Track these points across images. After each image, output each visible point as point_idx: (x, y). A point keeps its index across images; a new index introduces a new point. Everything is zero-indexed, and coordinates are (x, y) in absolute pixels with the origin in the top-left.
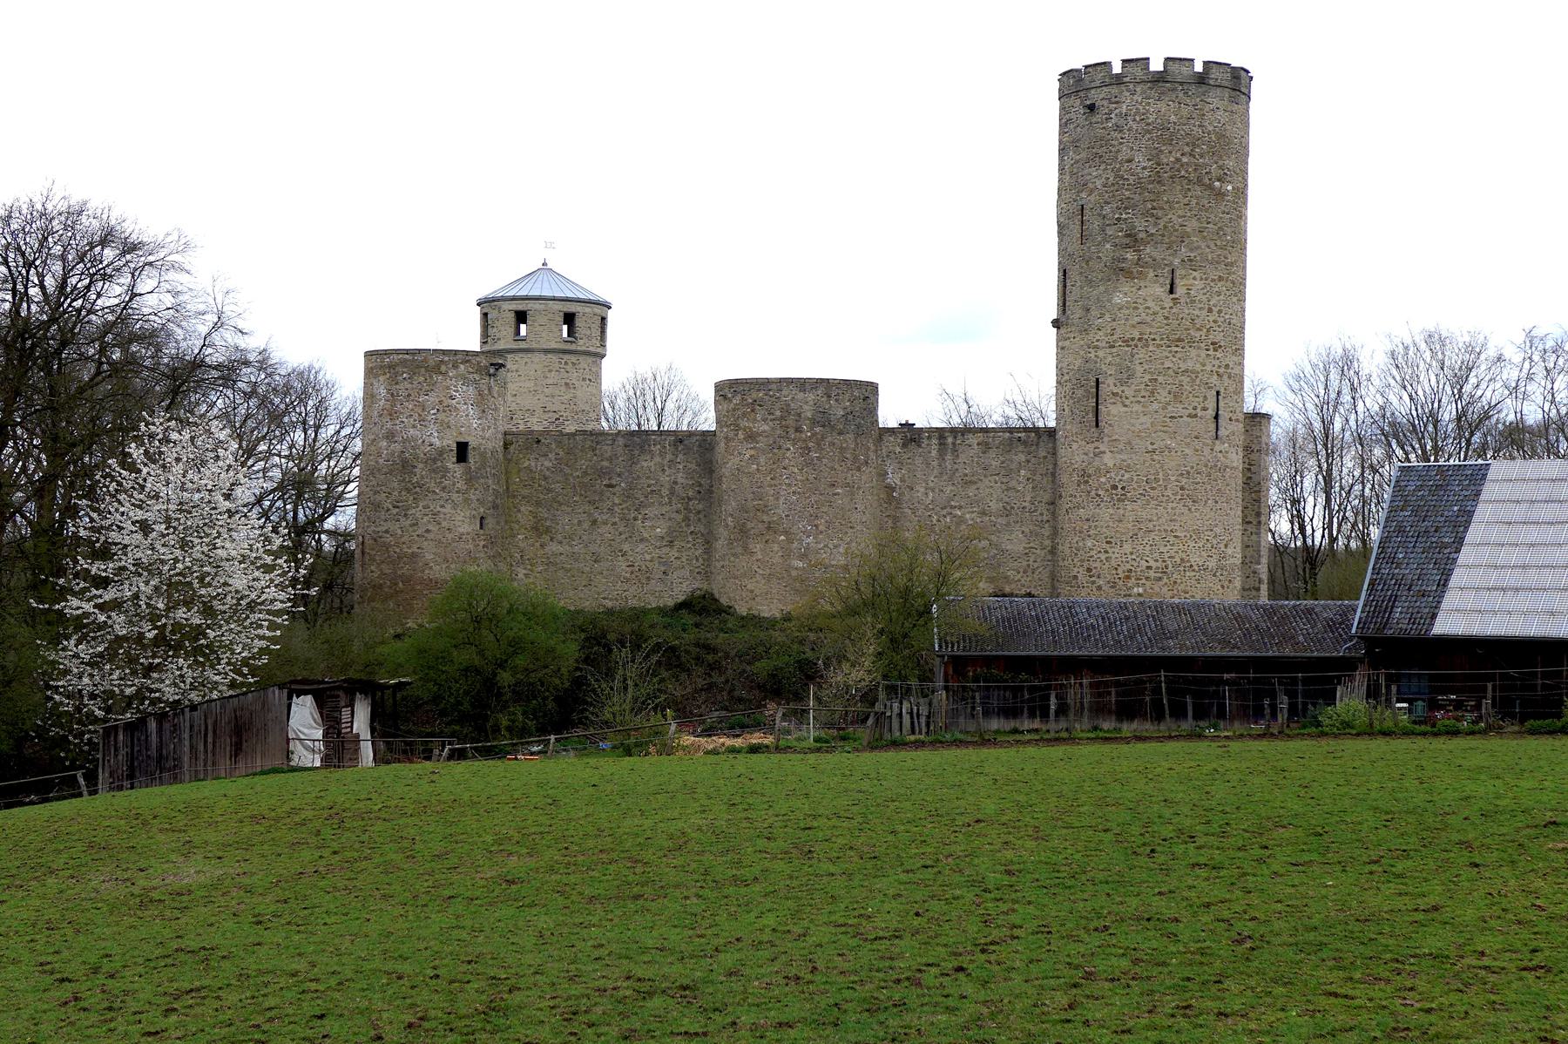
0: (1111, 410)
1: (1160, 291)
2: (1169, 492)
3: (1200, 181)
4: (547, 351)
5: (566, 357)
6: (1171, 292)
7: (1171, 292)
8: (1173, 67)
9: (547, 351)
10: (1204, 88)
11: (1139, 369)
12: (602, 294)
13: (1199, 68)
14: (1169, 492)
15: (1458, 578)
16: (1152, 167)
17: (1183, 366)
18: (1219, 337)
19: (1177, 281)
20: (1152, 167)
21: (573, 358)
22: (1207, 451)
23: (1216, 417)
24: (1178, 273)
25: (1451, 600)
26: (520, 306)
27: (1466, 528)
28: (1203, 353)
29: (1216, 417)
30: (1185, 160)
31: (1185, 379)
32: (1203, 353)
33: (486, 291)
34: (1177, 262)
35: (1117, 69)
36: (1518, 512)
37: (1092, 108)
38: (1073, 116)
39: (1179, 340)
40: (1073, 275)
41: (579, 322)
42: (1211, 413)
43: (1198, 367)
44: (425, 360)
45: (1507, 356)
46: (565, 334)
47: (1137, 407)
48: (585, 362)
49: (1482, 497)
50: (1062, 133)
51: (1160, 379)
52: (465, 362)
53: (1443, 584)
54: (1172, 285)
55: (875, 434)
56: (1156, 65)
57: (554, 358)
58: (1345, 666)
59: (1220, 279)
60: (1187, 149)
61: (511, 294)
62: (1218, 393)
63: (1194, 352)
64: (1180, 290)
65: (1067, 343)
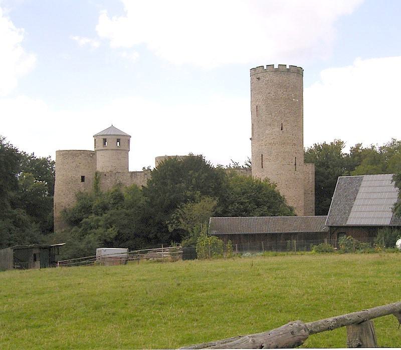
0: (266, 163)
1: (278, 129)
2: (283, 186)
4: (112, 150)
5: (118, 151)
6: (282, 130)
7: (282, 130)
8: (281, 67)
9: (112, 150)
10: (289, 73)
12: (127, 131)
14: (283, 186)
15: (354, 209)
16: (279, 91)
19: (283, 126)
20: (279, 91)
21: (120, 151)
22: (293, 174)
23: (295, 165)
24: (283, 124)
25: (352, 215)
26: (119, 138)
27: (357, 194)
28: (291, 147)
29: (295, 165)
30: (284, 93)
32: (291, 147)
33: (98, 130)
35: (276, 67)
36: (371, 189)
37: (259, 79)
38: (254, 81)
39: (284, 143)
40: (255, 126)
41: (121, 141)
42: (294, 163)
44: (72, 153)
45: (296, 211)
46: (118, 145)
47: (273, 162)
48: (123, 153)
49: (361, 186)
50: (251, 86)
52: (83, 153)
53: (350, 211)
55: (129, 175)
56: (276, 67)
57: (115, 151)
58: (325, 233)
59: (296, 126)
60: (285, 90)
61: (105, 134)
63: (288, 146)
65: (254, 145)
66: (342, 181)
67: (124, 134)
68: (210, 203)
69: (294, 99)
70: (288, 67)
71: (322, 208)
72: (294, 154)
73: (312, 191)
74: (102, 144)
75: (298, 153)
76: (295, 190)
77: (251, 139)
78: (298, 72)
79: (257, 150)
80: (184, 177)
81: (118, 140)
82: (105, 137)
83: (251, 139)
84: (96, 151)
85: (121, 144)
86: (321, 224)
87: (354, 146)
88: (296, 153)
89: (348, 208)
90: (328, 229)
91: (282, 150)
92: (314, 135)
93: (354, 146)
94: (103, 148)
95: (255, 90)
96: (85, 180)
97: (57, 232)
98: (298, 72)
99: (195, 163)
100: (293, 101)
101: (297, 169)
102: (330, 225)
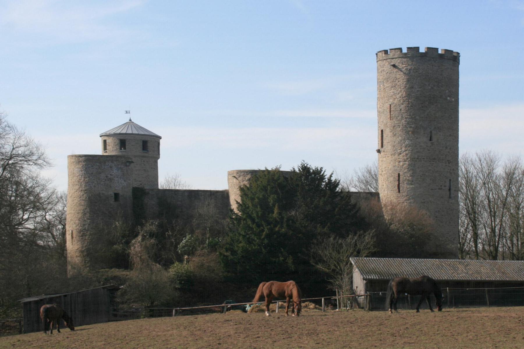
6: (430, 140)
12: (156, 131)
23: (450, 190)
24: (433, 132)
29: (450, 190)
30: (435, 88)
35: (422, 50)
39: (434, 159)
42: (447, 188)
54: (431, 137)
56: (422, 50)
59: (450, 135)
62: (450, 180)
64: (434, 139)
67: (151, 134)
69: (449, 98)
77: (379, 151)
78: (452, 59)
79: (397, 164)
88: (451, 173)
91: (430, 168)
95: (77, 169)
97: (44, 265)
98: (452, 59)
99: (318, 174)
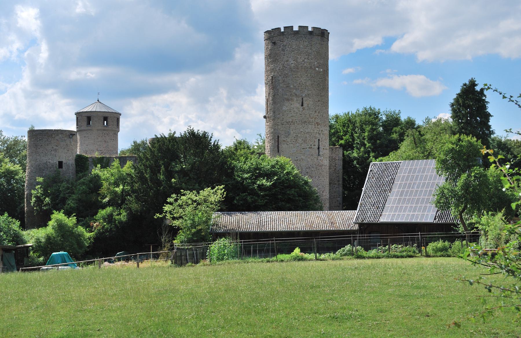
1: (299, 105)
3: (311, 67)
5: (105, 132)
7: (302, 105)
11: (292, 132)
13: (282, 30)
16: (297, 57)
17: (307, 131)
18: (319, 121)
22: (315, 160)
23: (319, 148)
24: (304, 99)
29: (319, 148)
30: (306, 60)
31: (307, 135)
34: (304, 95)
39: (305, 122)
41: (109, 120)
42: (317, 147)
43: (312, 131)
47: (291, 145)
51: (299, 135)
60: (306, 57)
63: (310, 126)
64: (305, 105)
66: (375, 165)
68: (214, 194)
69: (317, 69)
70: (310, 29)
71: (349, 201)
72: (317, 135)
73: (339, 181)
74: (86, 123)
75: (321, 134)
76: (319, 172)
77: (265, 117)
80: (187, 160)
81: (105, 119)
82: (89, 115)
83: (265, 117)
84: (76, 132)
85: (110, 123)
86: (345, 220)
87: (403, 118)
88: (319, 134)
89: (382, 201)
90: (356, 227)
92: (342, 102)
93: (403, 118)
94: (87, 128)
96: (64, 165)
98: (322, 35)
100: (316, 70)
101: (321, 153)
102: (360, 221)
